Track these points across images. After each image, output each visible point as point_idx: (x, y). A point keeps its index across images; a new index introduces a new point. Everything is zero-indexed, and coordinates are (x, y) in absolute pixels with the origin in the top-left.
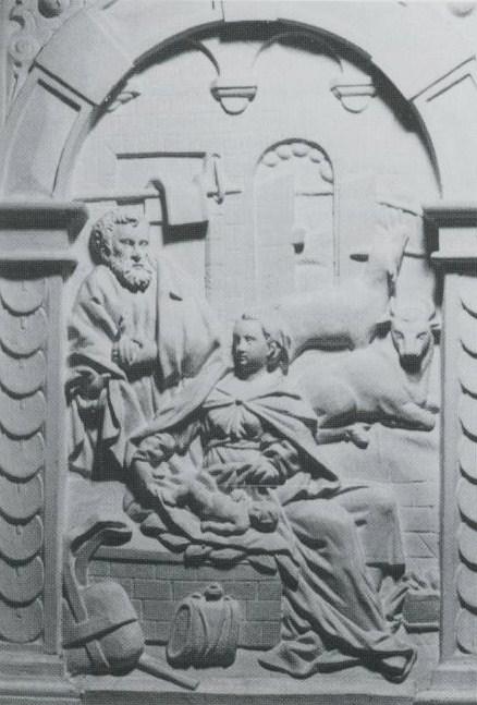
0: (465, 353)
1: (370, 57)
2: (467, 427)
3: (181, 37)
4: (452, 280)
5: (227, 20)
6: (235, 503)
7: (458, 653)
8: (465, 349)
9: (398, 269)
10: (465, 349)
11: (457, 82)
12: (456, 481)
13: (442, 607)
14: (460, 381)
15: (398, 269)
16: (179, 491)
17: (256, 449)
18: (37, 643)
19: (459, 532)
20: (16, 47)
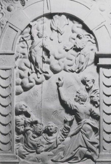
0: (104, 85)
1: (83, 22)
2: (104, 101)
3: (99, 65)
4: (101, 69)
5: (51, 13)
6: (70, 99)
7: (104, 150)
8: (104, 75)
9: (34, 26)
10: (104, 75)
11: (100, 27)
12: (103, 123)
13: (100, 103)
14: (103, 90)
15: (34, 26)
16: (16, 134)
17: (29, 126)
18: (10, 151)
19: (103, 124)
20: (2, 21)
